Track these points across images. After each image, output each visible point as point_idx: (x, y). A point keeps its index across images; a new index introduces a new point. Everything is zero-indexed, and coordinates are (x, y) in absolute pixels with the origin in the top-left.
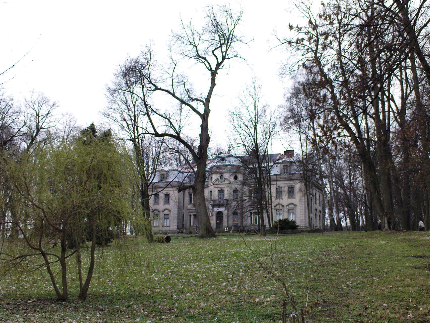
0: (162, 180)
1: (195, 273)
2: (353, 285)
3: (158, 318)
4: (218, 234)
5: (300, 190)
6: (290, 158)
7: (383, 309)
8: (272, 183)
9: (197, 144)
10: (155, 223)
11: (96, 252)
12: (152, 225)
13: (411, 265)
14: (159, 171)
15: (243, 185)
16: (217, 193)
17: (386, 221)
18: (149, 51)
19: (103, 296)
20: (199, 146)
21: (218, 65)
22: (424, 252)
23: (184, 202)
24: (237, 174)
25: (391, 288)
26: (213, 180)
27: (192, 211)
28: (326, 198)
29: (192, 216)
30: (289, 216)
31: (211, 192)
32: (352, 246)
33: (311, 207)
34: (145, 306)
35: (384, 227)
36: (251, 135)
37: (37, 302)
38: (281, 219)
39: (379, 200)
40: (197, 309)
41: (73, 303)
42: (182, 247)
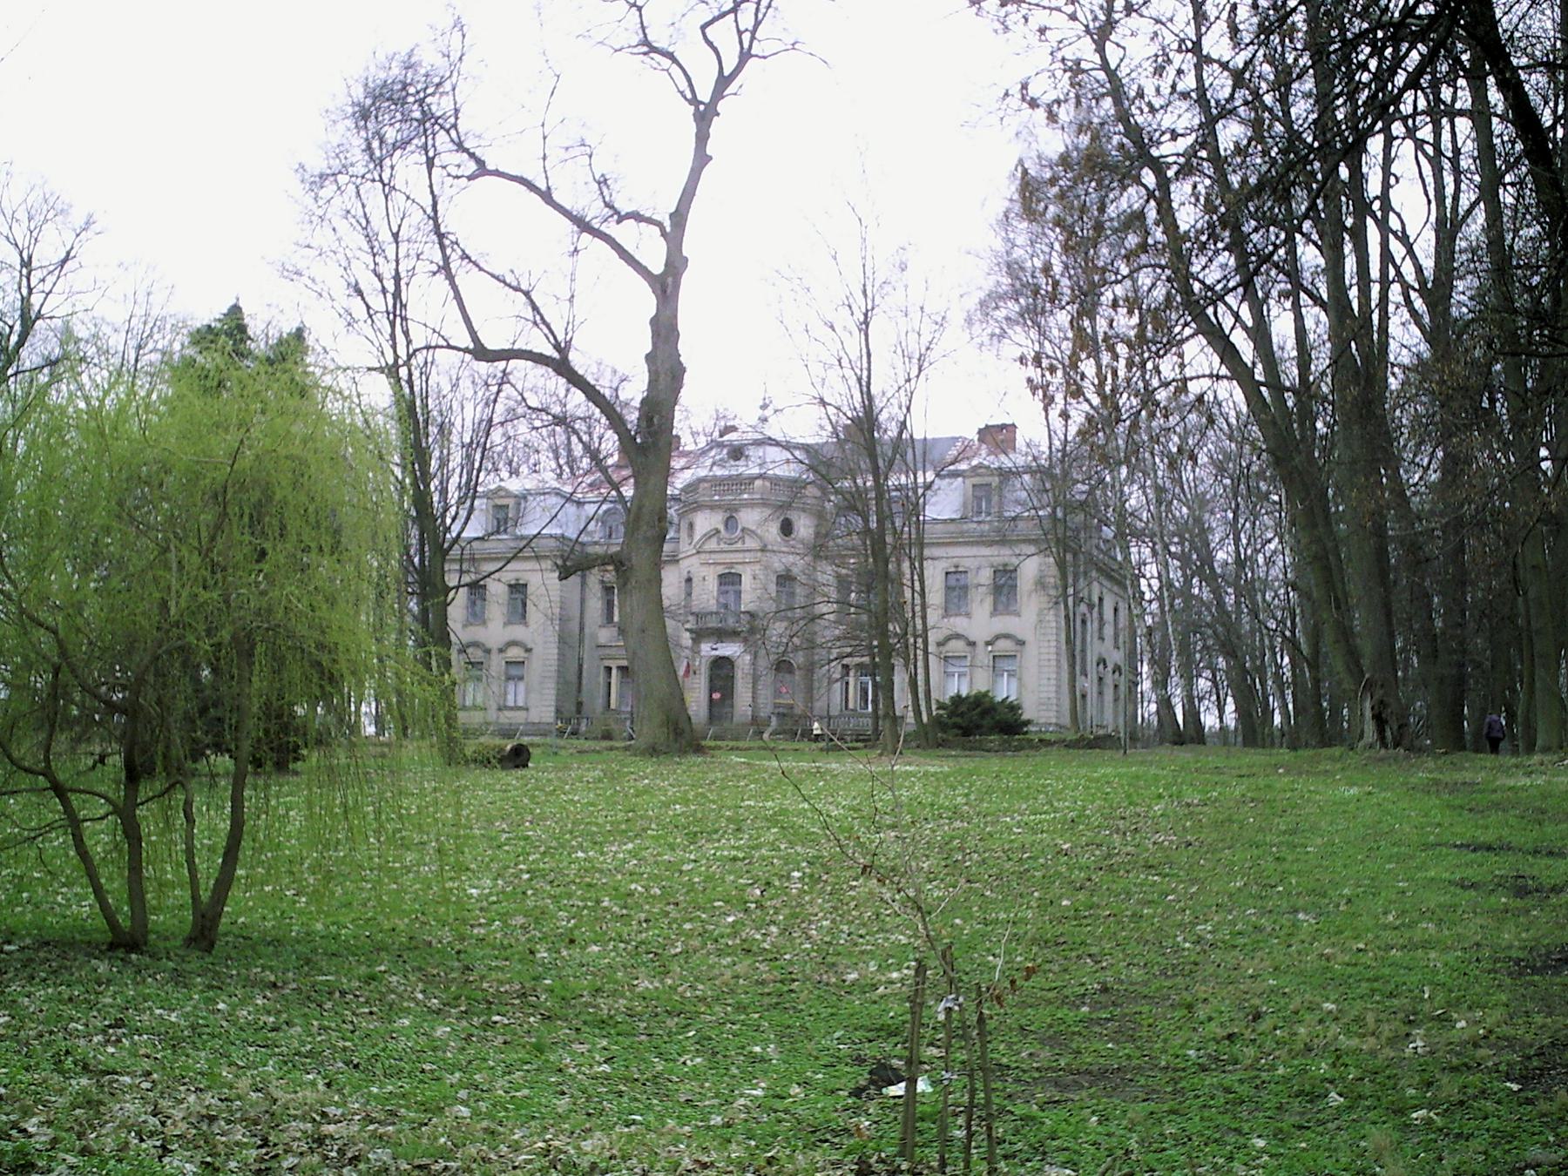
0: (498, 532)
1: (619, 877)
2: (1219, 936)
3: (475, 1021)
4: (713, 744)
5: (1041, 584)
6: (1003, 457)
7: (1321, 1021)
8: (927, 552)
9: (634, 391)
10: (471, 694)
11: (246, 793)
12: (458, 700)
13: (1446, 875)
14: (486, 495)
15: (817, 557)
16: (712, 585)
17: (1368, 714)
18: (459, 25)
19: (277, 942)
20: (643, 402)
21: (723, 81)
22: (1505, 832)
23: (582, 618)
24: (793, 516)
25: (1360, 950)
26: (697, 537)
27: (613, 652)
28: (1141, 617)
29: (614, 672)
30: (994, 682)
31: (689, 580)
32: (1231, 804)
33: (1083, 651)
34: (429, 980)
35: (1361, 736)
36: (845, 362)
37: (37, 950)
38: (964, 694)
39: (1345, 634)
40: (623, 996)
41: (169, 958)
42: (572, 787)
